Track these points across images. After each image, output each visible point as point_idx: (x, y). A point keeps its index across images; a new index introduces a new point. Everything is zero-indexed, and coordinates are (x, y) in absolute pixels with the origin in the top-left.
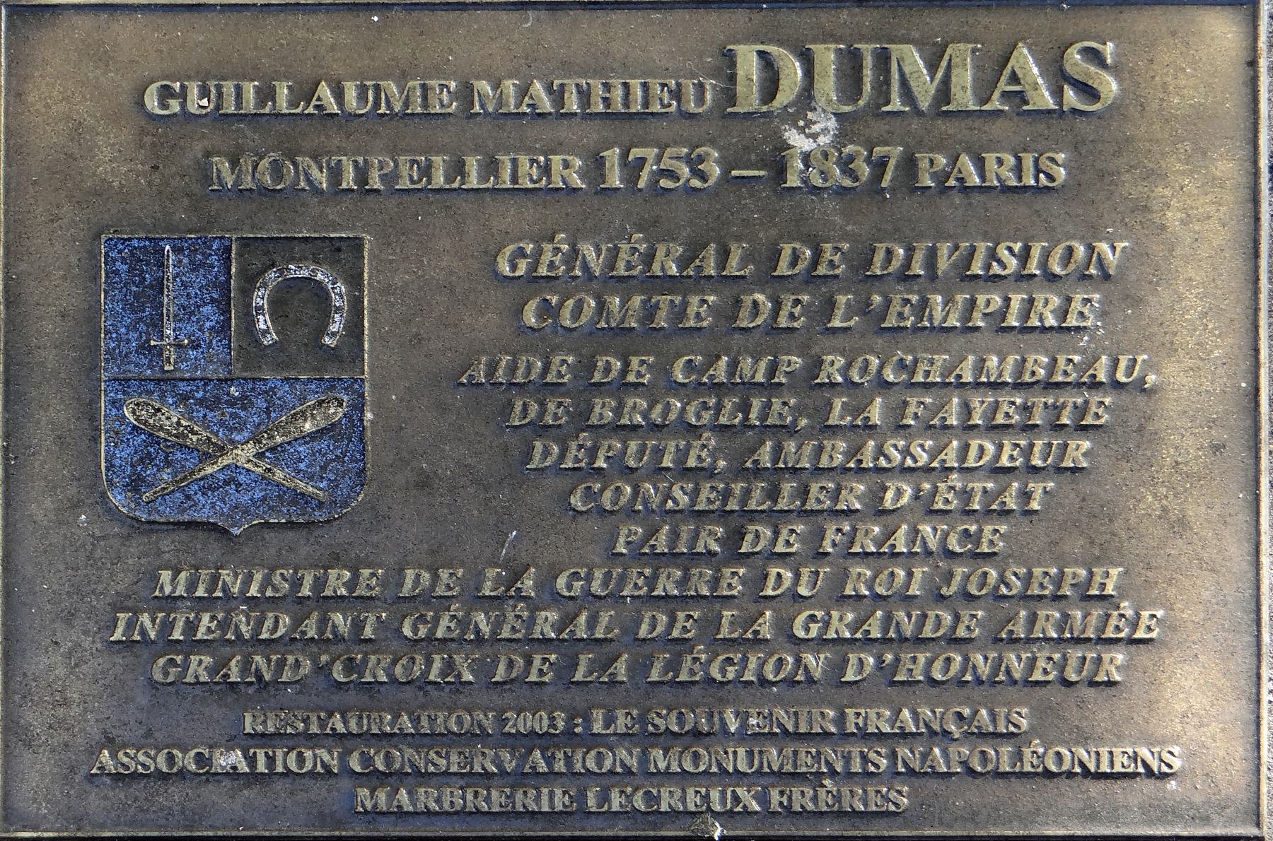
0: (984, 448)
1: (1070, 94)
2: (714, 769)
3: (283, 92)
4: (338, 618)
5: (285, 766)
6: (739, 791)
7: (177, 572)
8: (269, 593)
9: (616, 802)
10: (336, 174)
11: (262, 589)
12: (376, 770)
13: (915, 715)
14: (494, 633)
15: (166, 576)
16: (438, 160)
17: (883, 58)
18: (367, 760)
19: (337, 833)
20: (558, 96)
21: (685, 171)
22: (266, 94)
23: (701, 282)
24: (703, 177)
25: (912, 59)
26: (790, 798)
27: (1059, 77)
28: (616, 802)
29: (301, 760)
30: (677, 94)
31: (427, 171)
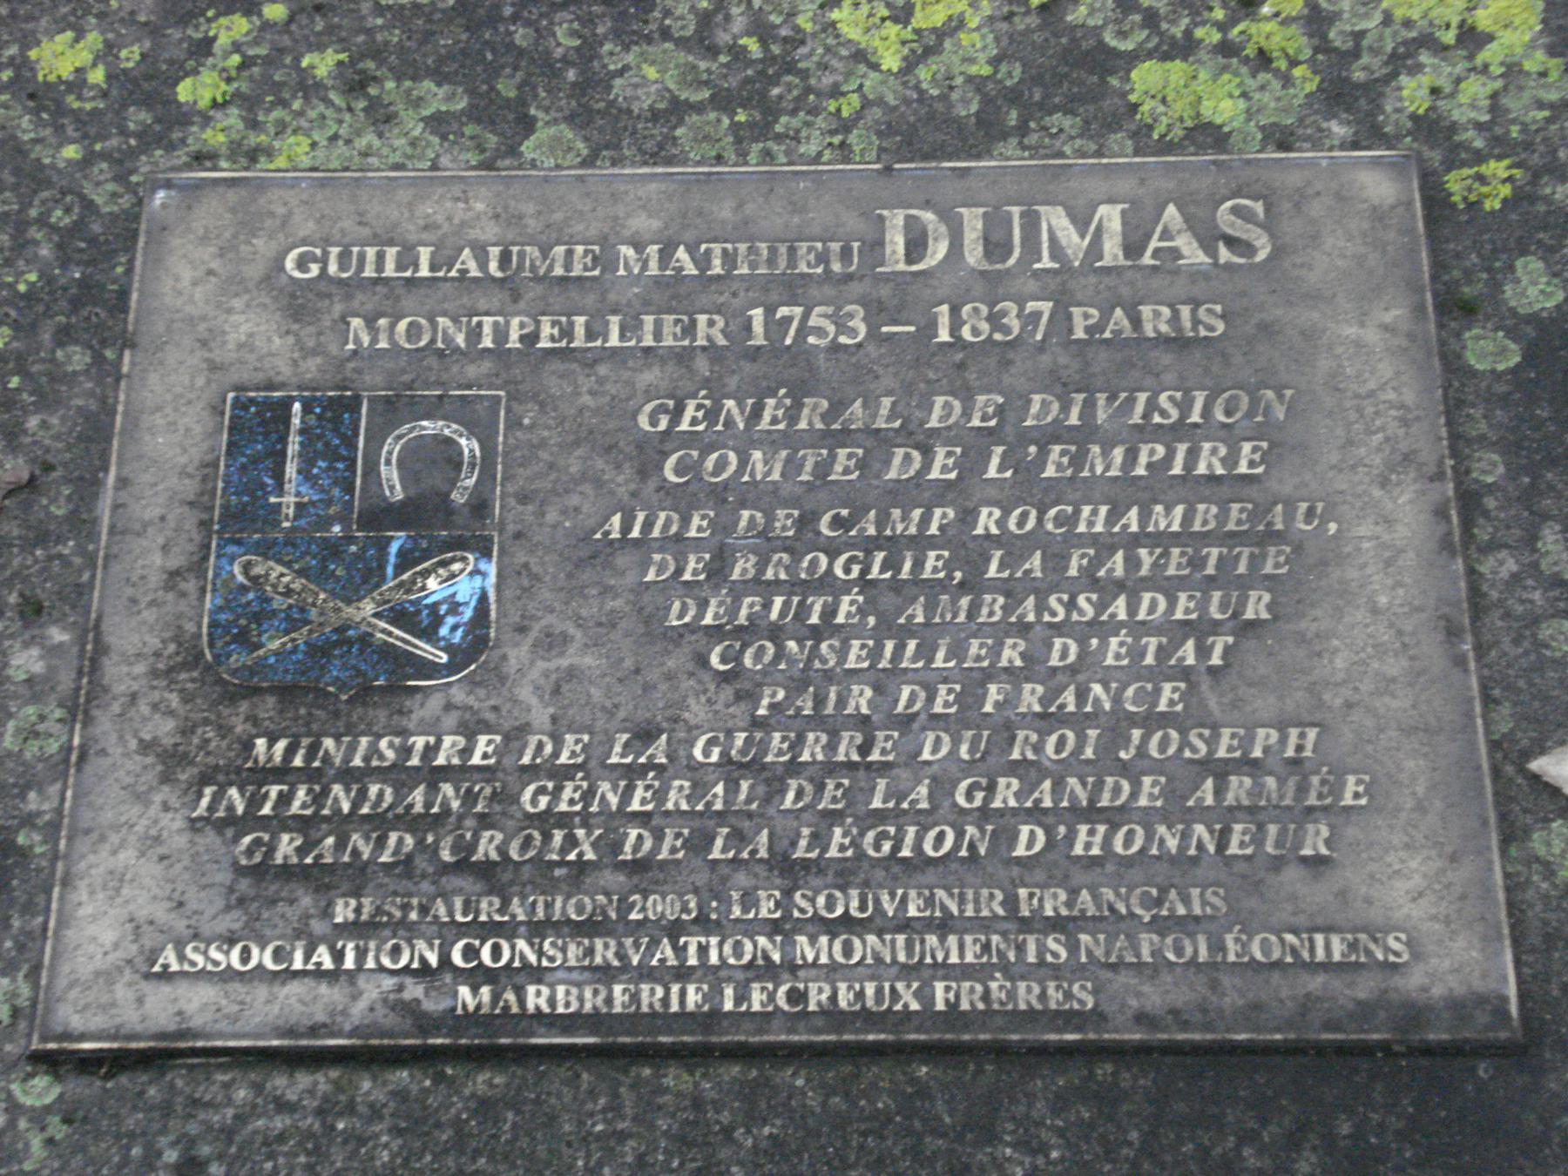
0: (1151, 605)
1: (1224, 254)
2: (1289, 959)
3: (425, 254)
4: (447, 789)
5: (830, 956)
6: (900, 986)
7: (272, 742)
8: (375, 763)
9: (757, 1000)
10: (475, 334)
11: (367, 759)
12: (1253, 959)
13: (1096, 897)
14: (1092, 801)
15: (261, 743)
16: (580, 321)
17: (1031, 223)
18: (470, 953)
19: (949, 1036)
20: (703, 262)
21: (831, 329)
22: (408, 259)
23: (844, 437)
24: (1006, 330)
25: (1055, 219)
26: (957, 996)
27: (1209, 238)
28: (757, 1000)
29: (848, 950)
30: (823, 258)
31: (567, 332)
